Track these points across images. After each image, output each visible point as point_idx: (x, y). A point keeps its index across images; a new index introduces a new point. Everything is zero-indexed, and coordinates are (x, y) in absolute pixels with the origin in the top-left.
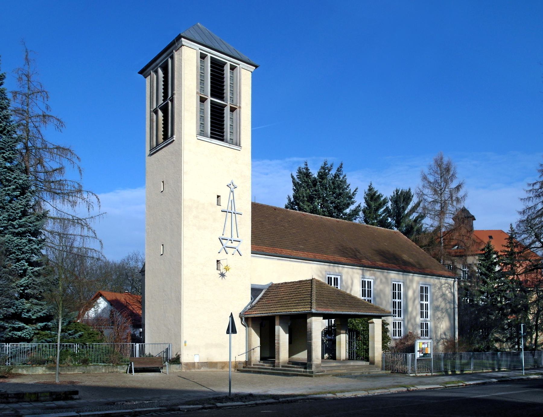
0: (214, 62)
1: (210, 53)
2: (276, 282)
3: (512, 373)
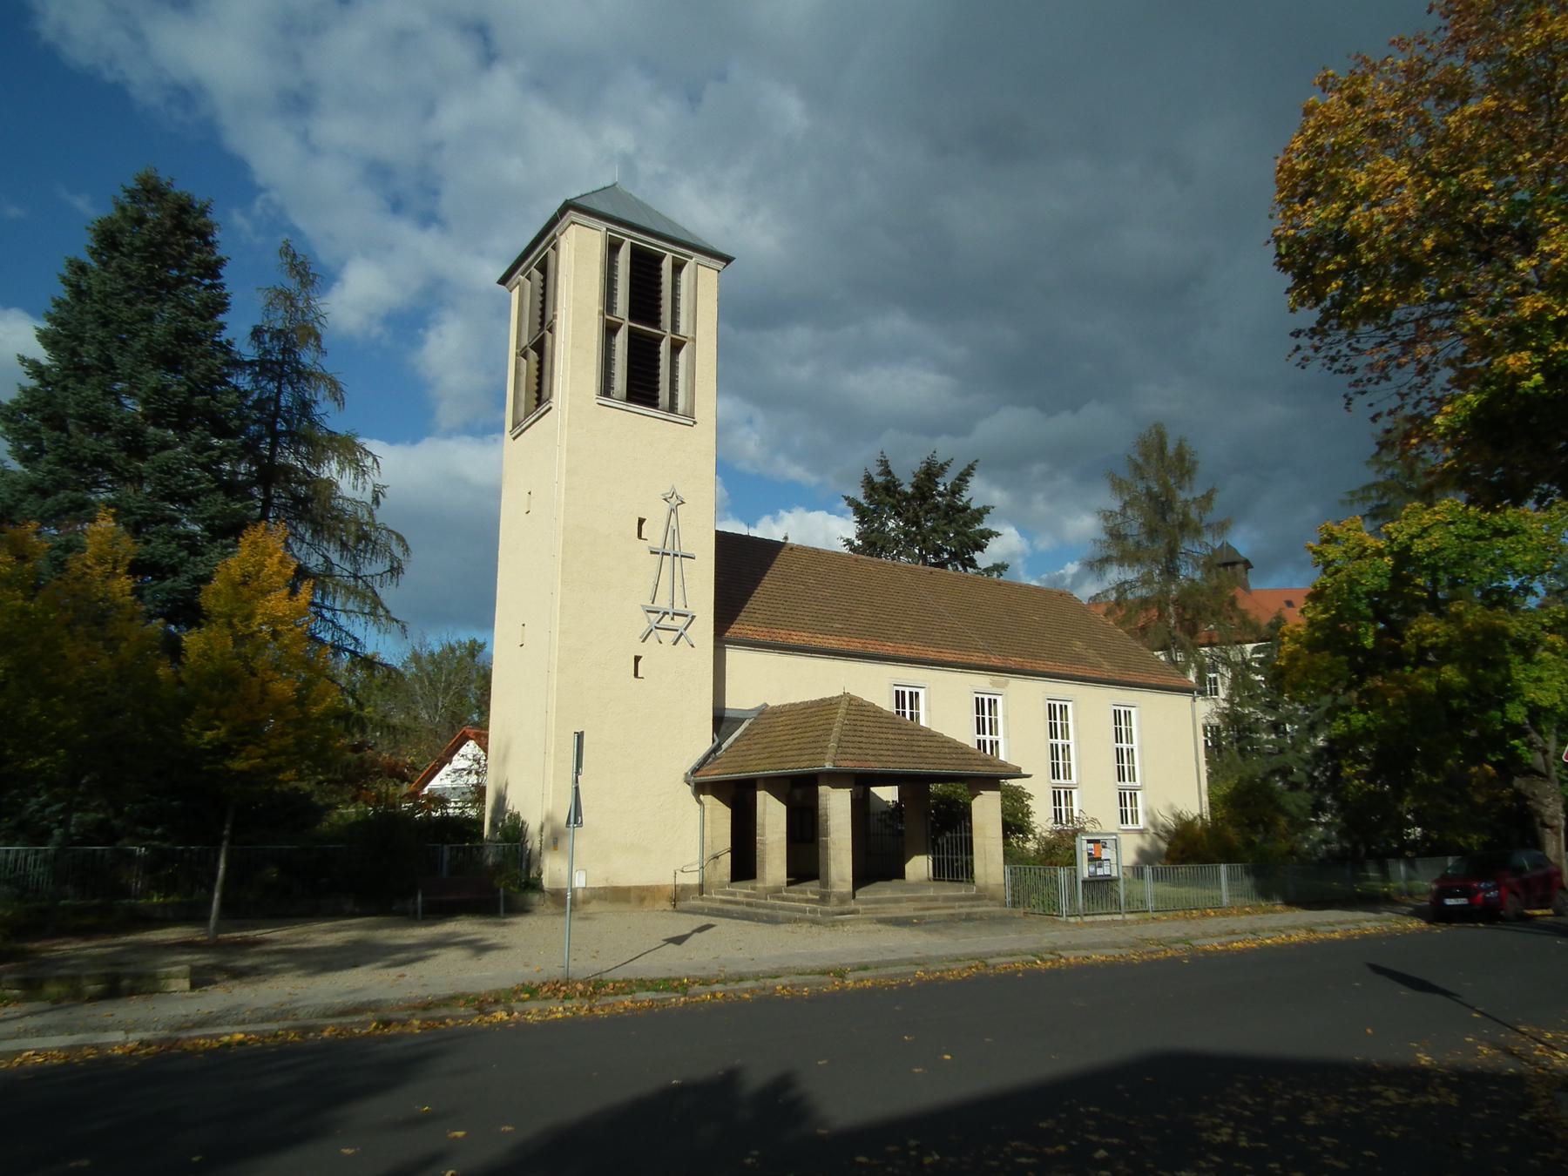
0: (636, 252)
2: (774, 702)
3: (1086, 857)
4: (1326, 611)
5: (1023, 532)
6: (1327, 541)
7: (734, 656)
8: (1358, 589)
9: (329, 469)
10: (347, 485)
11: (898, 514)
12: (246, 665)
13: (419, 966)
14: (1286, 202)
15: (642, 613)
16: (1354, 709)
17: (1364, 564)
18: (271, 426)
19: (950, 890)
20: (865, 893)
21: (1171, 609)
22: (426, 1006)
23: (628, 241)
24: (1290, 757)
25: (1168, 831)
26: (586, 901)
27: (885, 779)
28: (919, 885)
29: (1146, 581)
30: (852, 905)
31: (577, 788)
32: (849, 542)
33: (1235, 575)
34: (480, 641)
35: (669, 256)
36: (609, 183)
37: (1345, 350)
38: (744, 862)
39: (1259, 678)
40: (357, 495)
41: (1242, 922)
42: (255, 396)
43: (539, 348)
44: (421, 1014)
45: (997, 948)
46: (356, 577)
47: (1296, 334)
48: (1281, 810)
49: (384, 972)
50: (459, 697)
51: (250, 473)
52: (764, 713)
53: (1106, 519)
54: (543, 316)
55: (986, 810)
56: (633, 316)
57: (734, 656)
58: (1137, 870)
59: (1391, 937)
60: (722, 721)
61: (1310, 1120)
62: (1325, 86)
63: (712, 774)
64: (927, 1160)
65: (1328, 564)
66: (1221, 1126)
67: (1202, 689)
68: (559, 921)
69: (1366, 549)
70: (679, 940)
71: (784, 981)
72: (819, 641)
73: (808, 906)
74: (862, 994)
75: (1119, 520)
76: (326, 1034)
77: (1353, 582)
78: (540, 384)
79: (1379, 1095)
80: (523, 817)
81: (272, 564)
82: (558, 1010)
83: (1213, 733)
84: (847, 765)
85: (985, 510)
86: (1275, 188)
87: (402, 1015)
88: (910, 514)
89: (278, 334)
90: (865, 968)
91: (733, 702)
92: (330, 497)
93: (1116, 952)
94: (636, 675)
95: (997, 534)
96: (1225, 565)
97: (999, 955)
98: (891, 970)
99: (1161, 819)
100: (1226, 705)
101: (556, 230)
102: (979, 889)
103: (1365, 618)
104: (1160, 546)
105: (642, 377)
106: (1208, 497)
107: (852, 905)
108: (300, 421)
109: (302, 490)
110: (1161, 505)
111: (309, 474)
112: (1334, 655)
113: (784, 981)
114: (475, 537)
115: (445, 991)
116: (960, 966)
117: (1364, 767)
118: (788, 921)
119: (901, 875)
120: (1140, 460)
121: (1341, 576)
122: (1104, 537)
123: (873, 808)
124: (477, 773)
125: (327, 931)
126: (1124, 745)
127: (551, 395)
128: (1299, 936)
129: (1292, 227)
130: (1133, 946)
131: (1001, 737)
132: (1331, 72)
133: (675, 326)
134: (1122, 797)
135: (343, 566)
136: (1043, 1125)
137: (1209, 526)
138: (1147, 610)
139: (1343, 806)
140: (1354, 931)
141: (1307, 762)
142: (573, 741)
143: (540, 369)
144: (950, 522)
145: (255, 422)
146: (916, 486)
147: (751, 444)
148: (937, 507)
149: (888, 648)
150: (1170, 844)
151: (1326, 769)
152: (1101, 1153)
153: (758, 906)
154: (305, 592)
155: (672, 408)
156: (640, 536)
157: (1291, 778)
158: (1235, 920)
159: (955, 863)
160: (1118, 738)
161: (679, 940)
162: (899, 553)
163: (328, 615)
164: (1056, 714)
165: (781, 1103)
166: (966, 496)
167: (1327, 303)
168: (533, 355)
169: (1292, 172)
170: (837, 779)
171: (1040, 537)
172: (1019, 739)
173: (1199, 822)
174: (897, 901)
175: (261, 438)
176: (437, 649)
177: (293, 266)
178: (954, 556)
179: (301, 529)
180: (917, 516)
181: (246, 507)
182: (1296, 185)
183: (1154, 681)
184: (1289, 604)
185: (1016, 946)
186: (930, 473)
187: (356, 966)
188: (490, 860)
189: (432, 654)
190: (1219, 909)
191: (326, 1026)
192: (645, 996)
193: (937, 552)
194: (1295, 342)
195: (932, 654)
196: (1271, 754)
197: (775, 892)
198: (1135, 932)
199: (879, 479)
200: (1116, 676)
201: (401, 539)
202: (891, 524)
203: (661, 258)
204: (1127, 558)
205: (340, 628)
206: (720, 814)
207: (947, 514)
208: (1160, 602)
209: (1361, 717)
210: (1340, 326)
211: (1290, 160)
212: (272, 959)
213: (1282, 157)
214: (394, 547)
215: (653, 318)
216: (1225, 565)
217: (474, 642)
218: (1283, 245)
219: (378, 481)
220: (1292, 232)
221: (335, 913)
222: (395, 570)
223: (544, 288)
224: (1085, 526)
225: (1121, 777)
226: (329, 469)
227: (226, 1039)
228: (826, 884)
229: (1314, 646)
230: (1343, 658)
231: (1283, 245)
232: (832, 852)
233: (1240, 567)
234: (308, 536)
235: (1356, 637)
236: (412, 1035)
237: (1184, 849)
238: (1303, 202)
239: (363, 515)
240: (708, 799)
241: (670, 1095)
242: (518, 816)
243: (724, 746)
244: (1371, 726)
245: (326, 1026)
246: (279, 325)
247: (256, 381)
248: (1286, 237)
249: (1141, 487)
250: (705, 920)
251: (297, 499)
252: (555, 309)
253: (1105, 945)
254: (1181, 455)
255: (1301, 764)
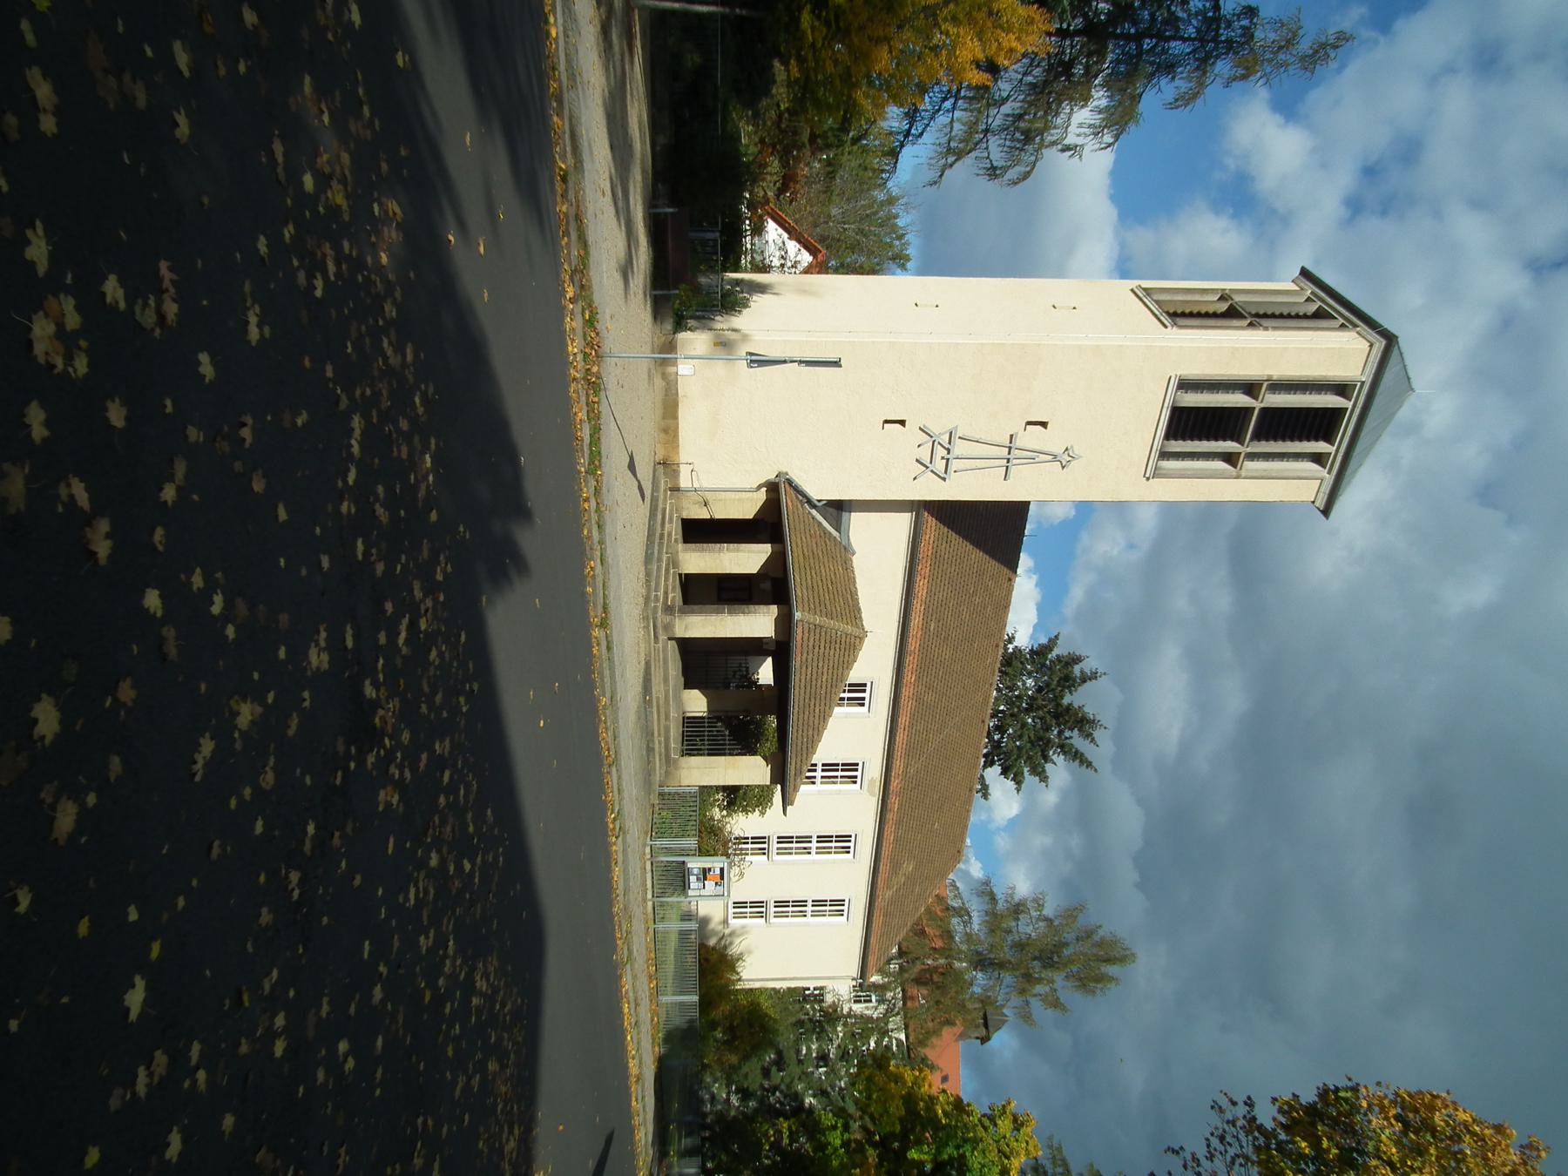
1: (1354, 406)
3: (707, 865)
4: (945, 1113)
5: (1013, 822)
6: (1015, 1120)
7: (904, 520)
8: (968, 1147)
9: (1100, 98)
10: (1080, 119)
11: (1039, 690)
12: (908, 20)
13: (612, 210)
14: (1397, 1099)
15: (950, 427)
16: (846, 1136)
17: (993, 1155)
18: (1147, 33)
19: (675, 732)
20: (672, 649)
21: (942, 961)
22: (578, 218)
23: (1349, 405)
24: (795, 1070)
25: (725, 947)
26: (664, 376)
27: (782, 672)
28: (679, 703)
29: (969, 937)
30: (662, 637)
31: (785, 362)
32: (1011, 640)
33: (977, 1027)
34: (909, 265)
35: (1331, 449)
36: (1414, 383)
37: (1232, 1152)
38: (701, 531)
39: (872, 1044)
40: (1073, 129)
41: (645, 1014)
42: (1181, 14)
43: (1231, 313)
44: (572, 212)
45: (625, 777)
46: (986, 131)
47: (1249, 1103)
48: (746, 1058)
49: (607, 175)
50: (851, 248)
51: (1097, 13)
52: (846, 551)
53: (1035, 900)
54: (1265, 316)
55: (751, 770)
56: (1266, 412)
57: (904, 520)
58: (687, 916)
59: (633, 1156)
60: (838, 509)
61: (492, 1066)
62: (1528, 1148)
63: (787, 499)
64: (462, 700)
65: (992, 1119)
66: (488, 980)
67: (863, 989)
68: (647, 348)
69: (1008, 1158)
70: (632, 467)
71: (599, 569)
72: (918, 607)
73: (661, 594)
74: (586, 644)
75: (1034, 914)
76: (555, 119)
77: (975, 1142)
78: (1191, 315)
79: (511, 1132)
80: (745, 311)
81: (1010, 41)
82: (574, 348)
83: (818, 996)
84: (798, 634)
85: (1044, 778)
86: (1413, 1090)
87: (571, 195)
88: (1040, 702)
89: (1248, 34)
90: (609, 648)
91: (857, 520)
92: (1071, 99)
93: (620, 891)
94: (887, 422)
95: (1018, 790)
96: (985, 1017)
97: (619, 778)
98: (607, 673)
99: (737, 941)
100: (846, 1010)
101: (1363, 327)
102: (675, 761)
103: (939, 1151)
104: (1006, 954)
105: (1197, 424)
106: (1056, 1004)
107: (662, 637)
108: (1152, 63)
109: (1078, 70)
110: (1049, 955)
111: (1096, 77)
112: (901, 1120)
113: (599, 569)
114: (1016, 256)
115: (591, 237)
116: (610, 739)
117: (786, 1141)
118: (648, 574)
119: (689, 685)
120: (1096, 938)
121: (981, 1132)
122: (1016, 899)
123: (752, 660)
124: (782, 266)
125: (640, 117)
126: (809, 908)
127: (1181, 327)
128: (633, 1066)
129: (1370, 1105)
130: (626, 908)
131: (819, 787)
132: (1543, 1154)
133: (1252, 456)
134: (759, 904)
135: (997, 118)
136: (489, 812)
137: (1027, 1003)
138: (941, 936)
139: (750, 1118)
140: (636, 1121)
141: (789, 1086)
142: (832, 357)
143: (1207, 315)
144: (1030, 741)
145: (1152, 15)
146: (1069, 708)
147: (1106, 546)
148: (1048, 729)
149: (909, 677)
150: (714, 948)
151: (782, 1104)
152: (467, 866)
153: (661, 544)
154: (977, 77)
155: (1164, 455)
156: (1029, 423)
157: (774, 1069)
158: (648, 1007)
159: (699, 738)
160: (816, 903)
161: (632, 467)
162: (999, 690)
163: (948, 104)
164: (843, 842)
165: (505, 563)
166: (1059, 759)
167: (1283, 1136)
168: (1223, 307)
169: (1432, 1108)
170: (785, 623)
171: (1011, 835)
172: (820, 806)
173: (735, 977)
174: (666, 680)
175: (1135, 23)
176: (900, 222)
177: (1323, 46)
178: (996, 746)
179: (1037, 72)
180: (1039, 708)
181: (1064, 11)
182: (1416, 1111)
183: (873, 940)
184: (945, 1079)
185: (626, 794)
186: (1084, 723)
187: (611, 147)
188: (703, 280)
189: (896, 217)
190: (657, 991)
191: (562, 119)
192: (585, 433)
193: (1000, 729)
194: (1240, 1098)
195: (903, 720)
196: (798, 1051)
197: (674, 562)
198: (637, 911)
199: (1077, 670)
200: (879, 903)
201: (1026, 175)
202: (1030, 682)
203: (1330, 441)
204: (994, 920)
205: (932, 118)
206: (747, 508)
207: (1041, 739)
208: (948, 951)
209: (838, 1142)
210: (1258, 1149)
211: (1446, 1107)
212: (618, 64)
213: (1449, 1098)
214: (1017, 169)
215: (1262, 434)
216: (985, 1017)
217: (908, 259)
218: (1349, 1094)
219: (1087, 150)
220: (1364, 1104)
221: (655, 126)
222: (993, 172)
223: (1297, 316)
224: (1020, 882)
225: (779, 904)
226: (1100, 98)
227: (552, 20)
228: (682, 612)
229: (910, 1100)
230: (898, 1128)
231: (1349, 1094)
232: (713, 618)
233: (983, 1032)
234: (1030, 79)
235: (919, 1142)
236: (555, 204)
237: (711, 963)
238: (1398, 1118)
239: (1053, 135)
240: (762, 496)
241: (512, 455)
242: (746, 306)
243: (814, 512)
244: (830, 1150)
245: (562, 119)
246: (1259, 34)
247: (1197, 14)
248: (1358, 1098)
249: (1069, 936)
250: (648, 493)
251: (1067, 68)
252: (1275, 328)
253: (626, 880)
254: (1101, 979)
255: (787, 1080)
